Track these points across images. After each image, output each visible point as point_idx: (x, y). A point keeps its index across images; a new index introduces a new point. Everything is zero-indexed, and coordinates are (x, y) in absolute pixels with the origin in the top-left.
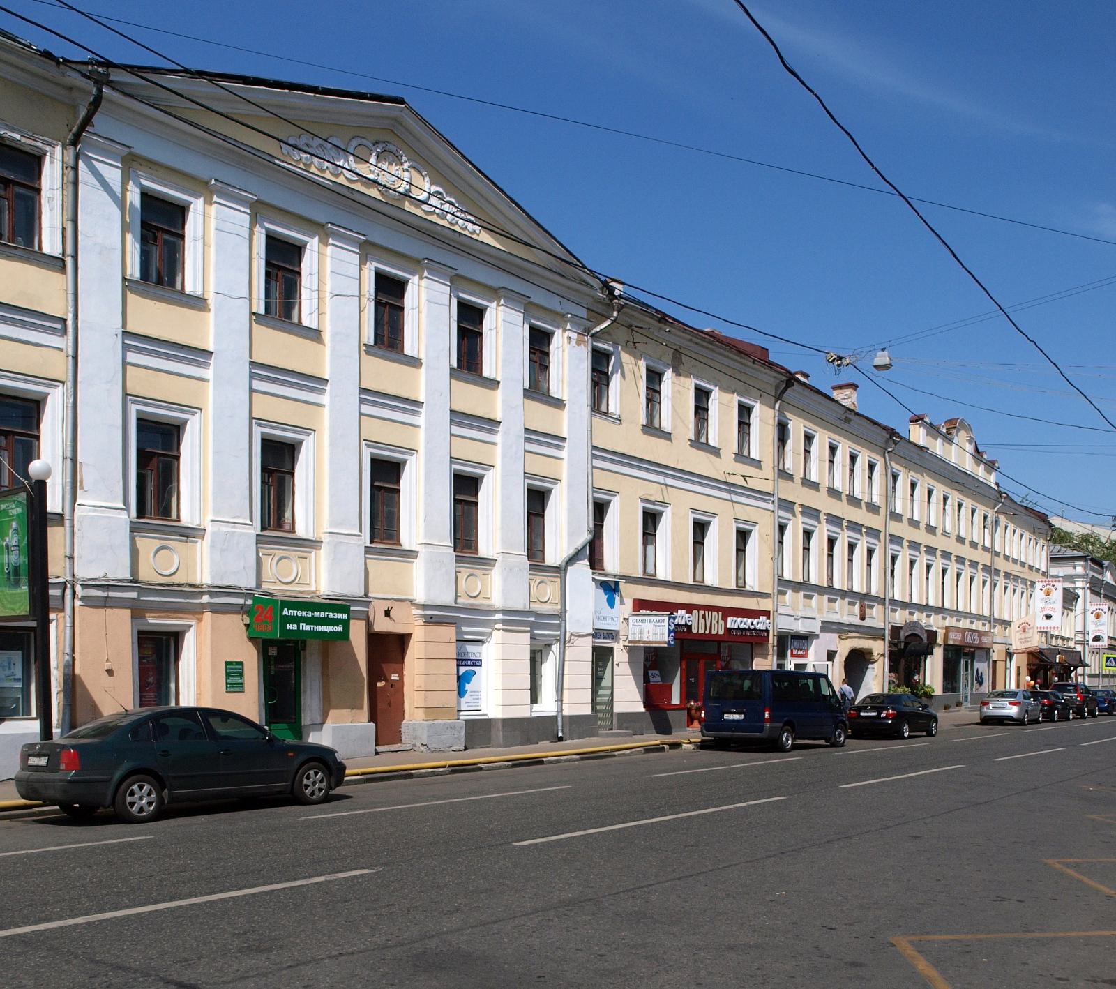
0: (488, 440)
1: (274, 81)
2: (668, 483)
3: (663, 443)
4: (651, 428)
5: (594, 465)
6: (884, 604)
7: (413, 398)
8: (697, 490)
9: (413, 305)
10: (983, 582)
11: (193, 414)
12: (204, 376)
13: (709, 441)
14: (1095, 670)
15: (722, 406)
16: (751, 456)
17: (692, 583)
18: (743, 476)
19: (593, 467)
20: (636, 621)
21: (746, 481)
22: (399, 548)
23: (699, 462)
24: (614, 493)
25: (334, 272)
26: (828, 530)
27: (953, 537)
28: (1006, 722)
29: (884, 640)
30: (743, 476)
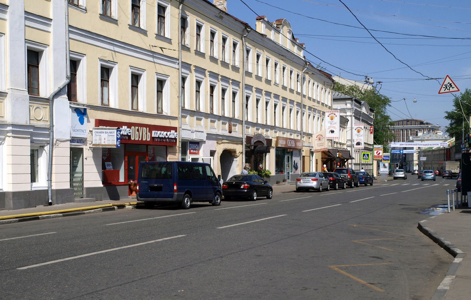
2: (116, 50)
5: (70, 37)
9: (168, 11)
13: (141, 26)
18: (160, 48)
19: (70, 38)
21: (162, 51)
30: (160, 48)
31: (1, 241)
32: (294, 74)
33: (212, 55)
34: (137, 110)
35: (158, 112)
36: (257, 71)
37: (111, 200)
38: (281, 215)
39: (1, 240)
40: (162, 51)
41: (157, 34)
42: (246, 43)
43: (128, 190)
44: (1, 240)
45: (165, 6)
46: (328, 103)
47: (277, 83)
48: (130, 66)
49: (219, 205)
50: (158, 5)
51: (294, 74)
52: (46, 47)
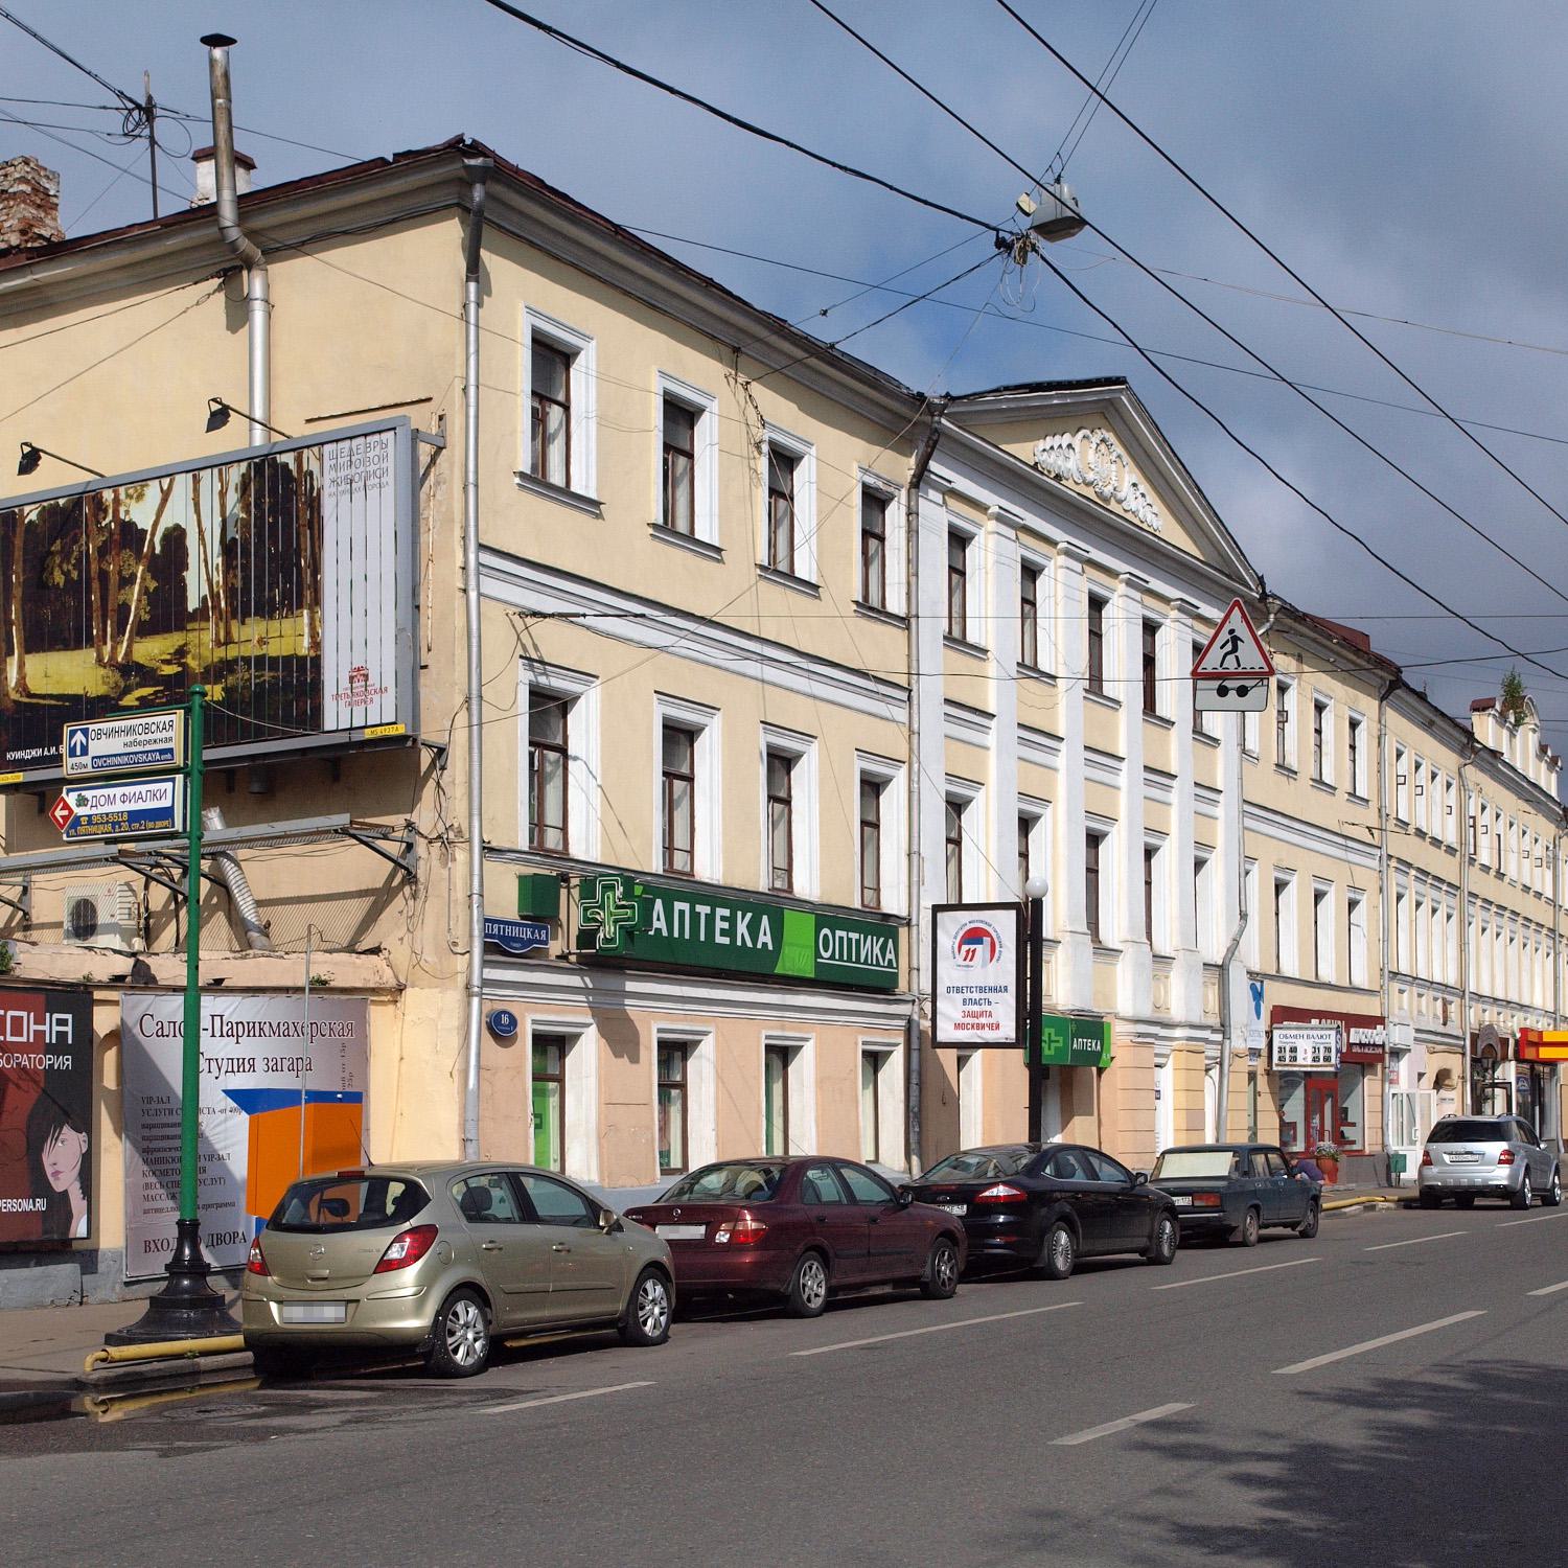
0: (975, 741)
1: (1078, 382)
2: (766, 678)
3: (799, 601)
4: (671, 529)
5: (1246, 825)
6: (1463, 997)
7: (1165, 770)
8: (1311, 847)
9: (899, 522)
10: (1277, 887)
11: (587, 684)
12: (1053, 765)
13: (1323, 778)
14: (51, 1038)
15: (1061, 588)
16: (574, 488)
17: (860, 908)
18: (1367, 827)
19: (1245, 828)
20: (1286, 1036)
21: (1372, 834)
22: (692, 879)
23: (776, 611)
24: (811, 739)
25: (1068, 598)
26: (1398, 884)
27: (1493, 873)
28: (1478, 1202)
29: (1464, 1054)
30: (1367, 827)
31: (4, 1398)
32: (817, 459)
33: (1281, 762)
34: (563, 854)
35: (863, 905)
36: (1033, 648)
37: (1438, 1124)
38: (1389, 1332)
39: (4, 1394)
40: (1372, 834)
41: (660, 521)
42: (946, 497)
43: (1228, 1142)
44: (4, 1394)
45: (567, 344)
46: (1056, 668)
47: (1326, 781)
48: (857, 749)
49: (1166, 1262)
50: (535, 341)
51: (716, 419)
52: (1112, 825)
